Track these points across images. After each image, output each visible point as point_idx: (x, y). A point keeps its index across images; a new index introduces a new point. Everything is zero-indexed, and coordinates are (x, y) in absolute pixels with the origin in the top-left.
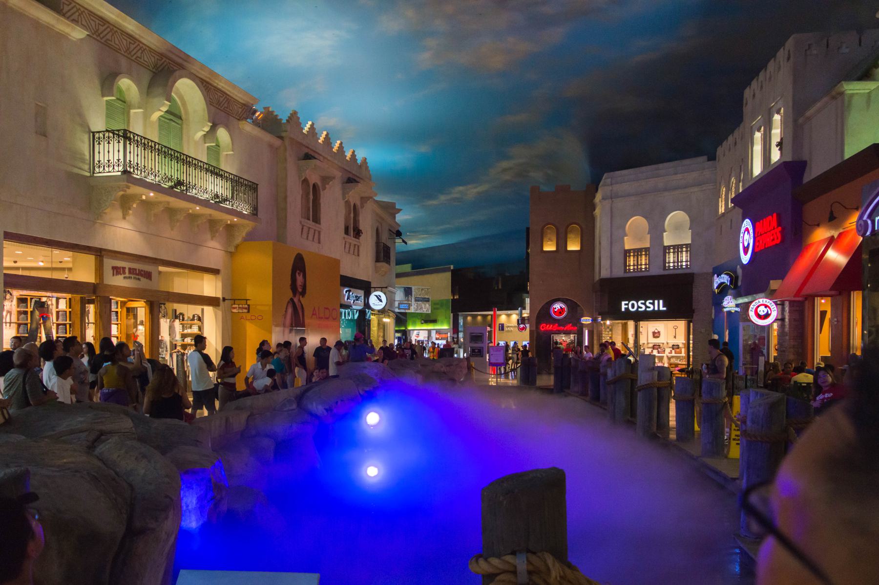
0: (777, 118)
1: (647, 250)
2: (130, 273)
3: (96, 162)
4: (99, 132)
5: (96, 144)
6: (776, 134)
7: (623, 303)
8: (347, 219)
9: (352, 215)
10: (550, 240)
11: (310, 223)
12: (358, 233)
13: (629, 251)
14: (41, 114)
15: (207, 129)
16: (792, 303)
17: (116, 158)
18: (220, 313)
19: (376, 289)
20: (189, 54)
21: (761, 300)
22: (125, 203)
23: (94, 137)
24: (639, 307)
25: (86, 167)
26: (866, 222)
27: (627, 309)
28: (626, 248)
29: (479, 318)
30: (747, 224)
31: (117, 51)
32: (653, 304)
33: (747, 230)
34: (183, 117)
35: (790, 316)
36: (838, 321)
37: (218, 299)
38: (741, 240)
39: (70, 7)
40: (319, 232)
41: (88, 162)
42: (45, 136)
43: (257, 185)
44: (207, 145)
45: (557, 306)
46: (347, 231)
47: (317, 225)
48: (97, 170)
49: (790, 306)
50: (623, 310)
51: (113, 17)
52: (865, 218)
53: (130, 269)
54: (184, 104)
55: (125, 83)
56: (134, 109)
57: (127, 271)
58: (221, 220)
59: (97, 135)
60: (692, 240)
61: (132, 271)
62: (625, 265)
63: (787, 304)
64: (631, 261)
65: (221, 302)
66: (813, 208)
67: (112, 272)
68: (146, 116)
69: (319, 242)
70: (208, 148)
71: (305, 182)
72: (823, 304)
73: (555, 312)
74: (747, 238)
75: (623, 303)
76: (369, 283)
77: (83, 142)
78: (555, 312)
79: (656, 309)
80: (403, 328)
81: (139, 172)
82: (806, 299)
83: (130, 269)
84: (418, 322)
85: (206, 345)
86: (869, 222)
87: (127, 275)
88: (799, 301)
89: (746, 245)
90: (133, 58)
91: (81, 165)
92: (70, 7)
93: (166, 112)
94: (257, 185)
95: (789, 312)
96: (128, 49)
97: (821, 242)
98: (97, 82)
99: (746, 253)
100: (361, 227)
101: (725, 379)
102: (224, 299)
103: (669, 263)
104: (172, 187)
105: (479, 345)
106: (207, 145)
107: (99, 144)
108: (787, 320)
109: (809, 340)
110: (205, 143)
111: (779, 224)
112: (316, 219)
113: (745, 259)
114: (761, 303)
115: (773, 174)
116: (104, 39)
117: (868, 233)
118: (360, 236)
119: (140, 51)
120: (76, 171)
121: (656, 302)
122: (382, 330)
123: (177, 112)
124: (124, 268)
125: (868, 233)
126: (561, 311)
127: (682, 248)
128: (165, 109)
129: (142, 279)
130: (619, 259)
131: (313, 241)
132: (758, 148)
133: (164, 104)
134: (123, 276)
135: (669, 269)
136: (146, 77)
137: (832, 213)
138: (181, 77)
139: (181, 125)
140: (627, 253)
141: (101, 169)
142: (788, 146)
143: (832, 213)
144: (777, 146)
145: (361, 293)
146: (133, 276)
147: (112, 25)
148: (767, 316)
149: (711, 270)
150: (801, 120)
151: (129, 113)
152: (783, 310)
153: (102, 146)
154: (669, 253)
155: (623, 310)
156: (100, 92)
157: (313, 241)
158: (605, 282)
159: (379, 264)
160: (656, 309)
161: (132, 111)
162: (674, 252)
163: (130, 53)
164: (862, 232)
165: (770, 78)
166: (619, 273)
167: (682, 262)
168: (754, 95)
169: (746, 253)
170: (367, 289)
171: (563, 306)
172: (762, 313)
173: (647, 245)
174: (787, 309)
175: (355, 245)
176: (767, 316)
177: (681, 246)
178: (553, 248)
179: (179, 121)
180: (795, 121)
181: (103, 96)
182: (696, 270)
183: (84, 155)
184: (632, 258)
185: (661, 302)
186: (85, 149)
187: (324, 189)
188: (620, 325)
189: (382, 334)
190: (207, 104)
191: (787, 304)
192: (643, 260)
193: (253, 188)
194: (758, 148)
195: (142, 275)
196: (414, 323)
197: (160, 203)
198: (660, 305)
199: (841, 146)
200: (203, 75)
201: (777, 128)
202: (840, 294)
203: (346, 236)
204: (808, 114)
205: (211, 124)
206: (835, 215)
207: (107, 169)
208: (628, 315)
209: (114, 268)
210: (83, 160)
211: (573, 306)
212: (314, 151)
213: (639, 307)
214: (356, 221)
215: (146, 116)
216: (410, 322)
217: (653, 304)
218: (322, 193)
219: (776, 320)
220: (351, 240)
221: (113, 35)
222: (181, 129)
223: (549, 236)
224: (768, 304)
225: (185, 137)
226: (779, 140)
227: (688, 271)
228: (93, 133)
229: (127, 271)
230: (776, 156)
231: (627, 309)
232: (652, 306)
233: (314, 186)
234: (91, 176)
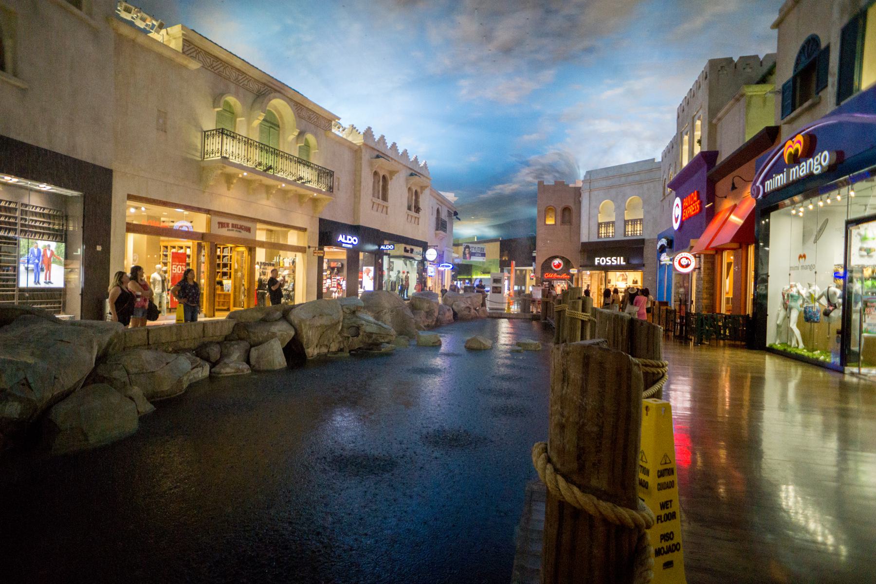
0: (698, 123)
1: (613, 223)
2: (233, 227)
3: (206, 151)
4: (208, 131)
5: (206, 138)
6: (698, 134)
7: (596, 259)
8: (409, 200)
9: (414, 198)
10: (551, 217)
11: (380, 201)
12: (417, 210)
13: (601, 224)
14: (162, 115)
15: (296, 134)
16: (706, 256)
17: (217, 148)
18: (306, 257)
19: (431, 247)
20: (286, 83)
21: (686, 254)
22: (229, 179)
23: (206, 135)
24: (607, 262)
25: (199, 154)
26: (758, 188)
27: (599, 263)
28: (600, 221)
29: (518, 272)
30: (678, 201)
31: (229, 79)
32: (616, 260)
33: (677, 205)
34: (280, 126)
35: (704, 266)
36: (738, 269)
37: (305, 247)
38: (674, 213)
39: (190, 48)
40: (387, 207)
41: (200, 151)
42: (166, 132)
43: (333, 172)
44: (299, 145)
45: (557, 261)
46: (409, 208)
47: (385, 202)
48: (206, 156)
49: (705, 258)
50: (596, 264)
51: (224, 56)
52: (758, 184)
53: (233, 224)
54: (281, 117)
55: (231, 99)
56: (239, 117)
57: (230, 226)
58: (307, 195)
59: (207, 133)
60: (644, 216)
61: (233, 225)
62: (599, 233)
63: (702, 256)
64: (603, 230)
65: (307, 249)
66: (723, 186)
67: (217, 225)
68: (249, 123)
69: (387, 214)
70: (300, 147)
71: (376, 174)
72: (728, 257)
73: (555, 266)
74: (677, 212)
75: (596, 259)
76: (427, 243)
77: (196, 137)
78: (555, 266)
79: (619, 263)
80: (470, 277)
81: (234, 158)
82: (717, 253)
83: (233, 224)
84: (479, 273)
85: (767, 315)
86: (761, 187)
87: (230, 228)
88: (711, 255)
89: (676, 216)
90: (241, 85)
91: (194, 152)
92: (190, 48)
93: (263, 120)
94: (333, 172)
95: (704, 263)
96: (237, 79)
97: (728, 209)
98: (210, 100)
99: (676, 222)
100: (421, 206)
101: (131, 279)
102: (309, 247)
103: (628, 231)
104: (295, 181)
105: (495, 285)
106: (299, 145)
107: (208, 139)
108: (702, 269)
109: (718, 282)
110: (297, 144)
111: (698, 198)
112: (385, 198)
113: (676, 226)
114: (683, 256)
115: (695, 164)
116: (218, 70)
117: (760, 196)
118: (419, 211)
119: (247, 81)
120: (189, 156)
121: (618, 258)
122: (440, 275)
123: (275, 123)
124: (228, 224)
125: (760, 196)
126: (559, 265)
127: (637, 221)
128: (262, 118)
129: (243, 232)
130: (594, 229)
131: (377, 211)
132: (686, 147)
133: (260, 115)
134: (226, 229)
135: (628, 236)
136: (250, 98)
137: (733, 184)
138: (275, 97)
139: (279, 131)
140: (599, 225)
141: (208, 156)
142: (705, 142)
143: (733, 184)
144: (698, 142)
145: (421, 249)
146: (235, 229)
147: (224, 62)
148: (688, 265)
149: (657, 237)
150: (714, 121)
151: (235, 121)
152: (700, 261)
153: (209, 140)
154: (628, 225)
155: (596, 264)
156: (212, 105)
157: (377, 211)
158: (584, 245)
159: (438, 232)
160: (619, 263)
161: (238, 119)
162: (632, 225)
163: (238, 81)
164: (755, 195)
165: (694, 95)
166: (594, 239)
167: (637, 231)
168: (683, 110)
169: (676, 222)
170: (425, 246)
171: (560, 262)
172: (684, 263)
173: (613, 219)
174: (702, 260)
175: (416, 217)
176: (688, 265)
177: (636, 220)
178: (553, 222)
179: (278, 129)
180: (710, 123)
181: (214, 107)
182: (646, 237)
183: (197, 146)
184: (603, 228)
185: (622, 258)
186: (198, 142)
187: (391, 179)
188: (597, 275)
189: (440, 278)
190: (296, 117)
191: (702, 256)
192: (611, 230)
193: (330, 174)
194: (686, 147)
195: (242, 229)
196: (477, 274)
197: (291, 190)
198: (621, 261)
199: (744, 138)
200: (297, 99)
201: (698, 131)
202: (741, 247)
203: (408, 211)
204: (719, 115)
205: (299, 131)
206: (736, 186)
207: (211, 155)
208: (600, 268)
209: (219, 223)
210: (196, 150)
211: (568, 264)
212: (383, 154)
213: (607, 262)
214: (417, 201)
215: (249, 123)
216: (474, 273)
217: (616, 260)
218: (390, 183)
219: (695, 269)
220: (413, 213)
221: (212, 65)
222: (279, 134)
223: (550, 214)
224: (689, 257)
225: (281, 140)
226: (699, 138)
227: (641, 237)
228: (205, 132)
229: (230, 226)
230: (697, 150)
231: (599, 263)
232: (615, 261)
233: (384, 177)
234: (202, 161)
